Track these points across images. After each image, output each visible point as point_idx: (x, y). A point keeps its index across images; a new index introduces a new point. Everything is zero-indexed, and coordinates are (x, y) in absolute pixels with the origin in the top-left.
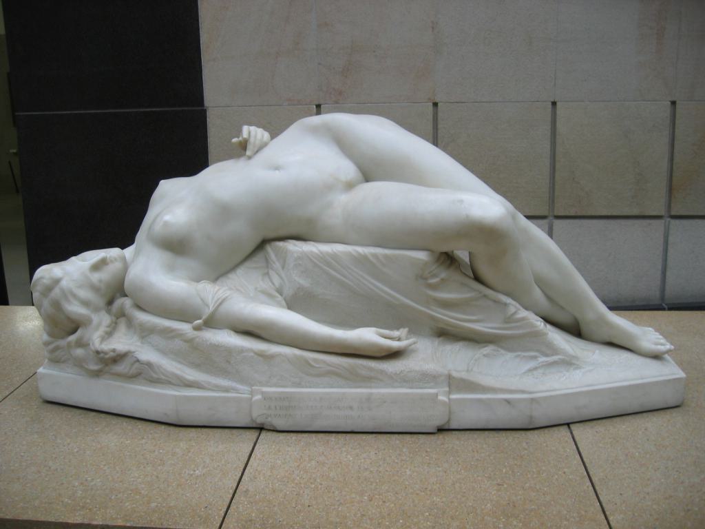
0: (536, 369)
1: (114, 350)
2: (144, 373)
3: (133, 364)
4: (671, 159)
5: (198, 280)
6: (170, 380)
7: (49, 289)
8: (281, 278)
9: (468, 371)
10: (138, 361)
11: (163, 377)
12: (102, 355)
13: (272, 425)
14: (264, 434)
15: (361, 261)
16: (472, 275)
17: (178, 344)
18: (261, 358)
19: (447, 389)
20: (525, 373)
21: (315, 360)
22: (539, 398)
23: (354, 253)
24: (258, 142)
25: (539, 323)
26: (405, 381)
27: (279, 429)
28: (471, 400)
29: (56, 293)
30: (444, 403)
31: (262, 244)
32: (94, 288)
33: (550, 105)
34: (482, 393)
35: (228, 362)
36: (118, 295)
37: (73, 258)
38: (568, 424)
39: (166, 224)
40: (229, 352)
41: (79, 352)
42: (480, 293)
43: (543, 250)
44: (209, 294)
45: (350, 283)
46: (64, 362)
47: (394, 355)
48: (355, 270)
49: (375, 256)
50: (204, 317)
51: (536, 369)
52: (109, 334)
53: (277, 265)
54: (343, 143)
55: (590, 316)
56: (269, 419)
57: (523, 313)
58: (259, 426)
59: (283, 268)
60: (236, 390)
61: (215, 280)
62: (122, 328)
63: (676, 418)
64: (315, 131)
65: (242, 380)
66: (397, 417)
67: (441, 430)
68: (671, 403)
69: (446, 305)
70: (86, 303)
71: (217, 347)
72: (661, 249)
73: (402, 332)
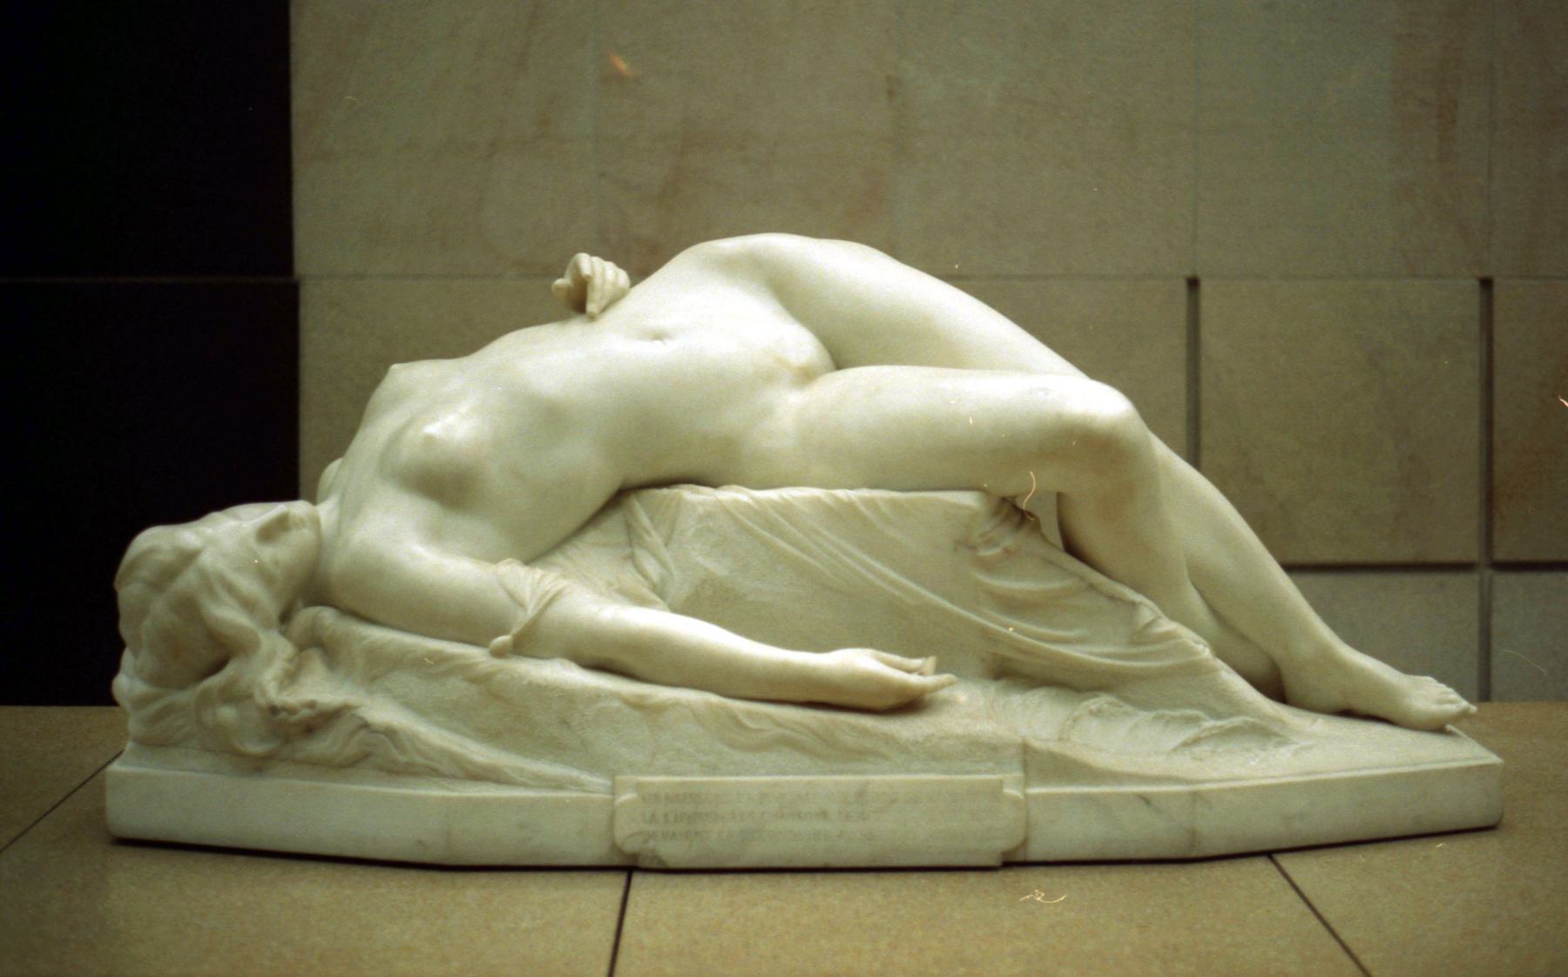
0: (1196, 741)
1: (311, 705)
2: (379, 755)
3: (353, 733)
4: (1488, 423)
5: (495, 559)
6: (432, 764)
7: (169, 573)
8: (663, 564)
9: (1060, 739)
10: (365, 725)
11: (420, 760)
12: (283, 715)
13: (656, 857)
14: (638, 879)
15: (842, 516)
16: (1059, 543)
17: (456, 687)
18: (637, 714)
19: (1019, 774)
20: (1175, 750)
21: (750, 715)
22: (1212, 791)
23: (828, 500)
24: (608, 287)
25: (1200, 647)
26: (934, 758)
27: (672, 864)
28: (1071, 796)
29: (188, 580)
30: (1015, 802)
31: (620, 497)
32: (264, 575)
33: (1182, 287)
34: (1089, 784)
35: (565, 723)
36: (300, 604)
37: (216, 516)
38: (1269, 854)
39: (429, 440)
40: (568, 697)
41: (227, 713)
42: (1082, 579)
43: (1197, 509)
44: (524, 585)
45: (818, 565)
46: (176, 744)
47: (909, 704)
48: (825, 533)
49: (869, 502)
50: (515, 630)
51: (1196, 741)
52: (291, 677)
53: (655, 539)
54: (789, 292)
55: (1304, 650)
56: (651, 844)
57: (1167, 625)
58: (626, 862)
59: (667, 542)
60: (578, 785)
61: (530, 561)
62: (317, 666)
63: (1490, 843)
64: (729, 267)
65: (594, 765)
66: (919, 834)
67: (1012, 863)
68: (1476, 819)
69: (1013, 606)
70: (248, 605)
71: (543, 692)
72: (1475, 647)
73: (929, 663)
